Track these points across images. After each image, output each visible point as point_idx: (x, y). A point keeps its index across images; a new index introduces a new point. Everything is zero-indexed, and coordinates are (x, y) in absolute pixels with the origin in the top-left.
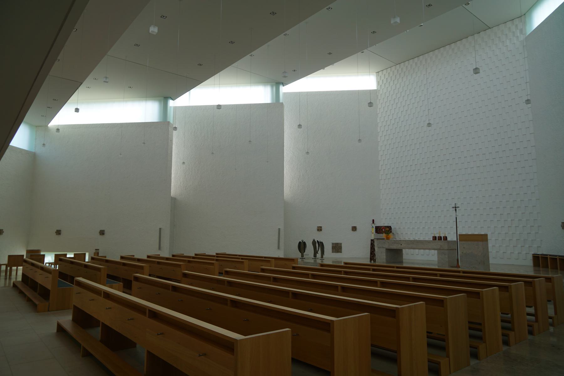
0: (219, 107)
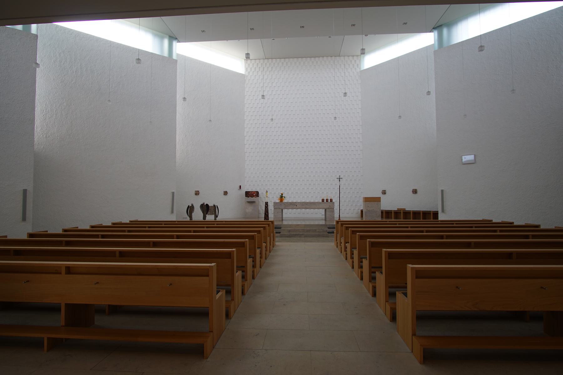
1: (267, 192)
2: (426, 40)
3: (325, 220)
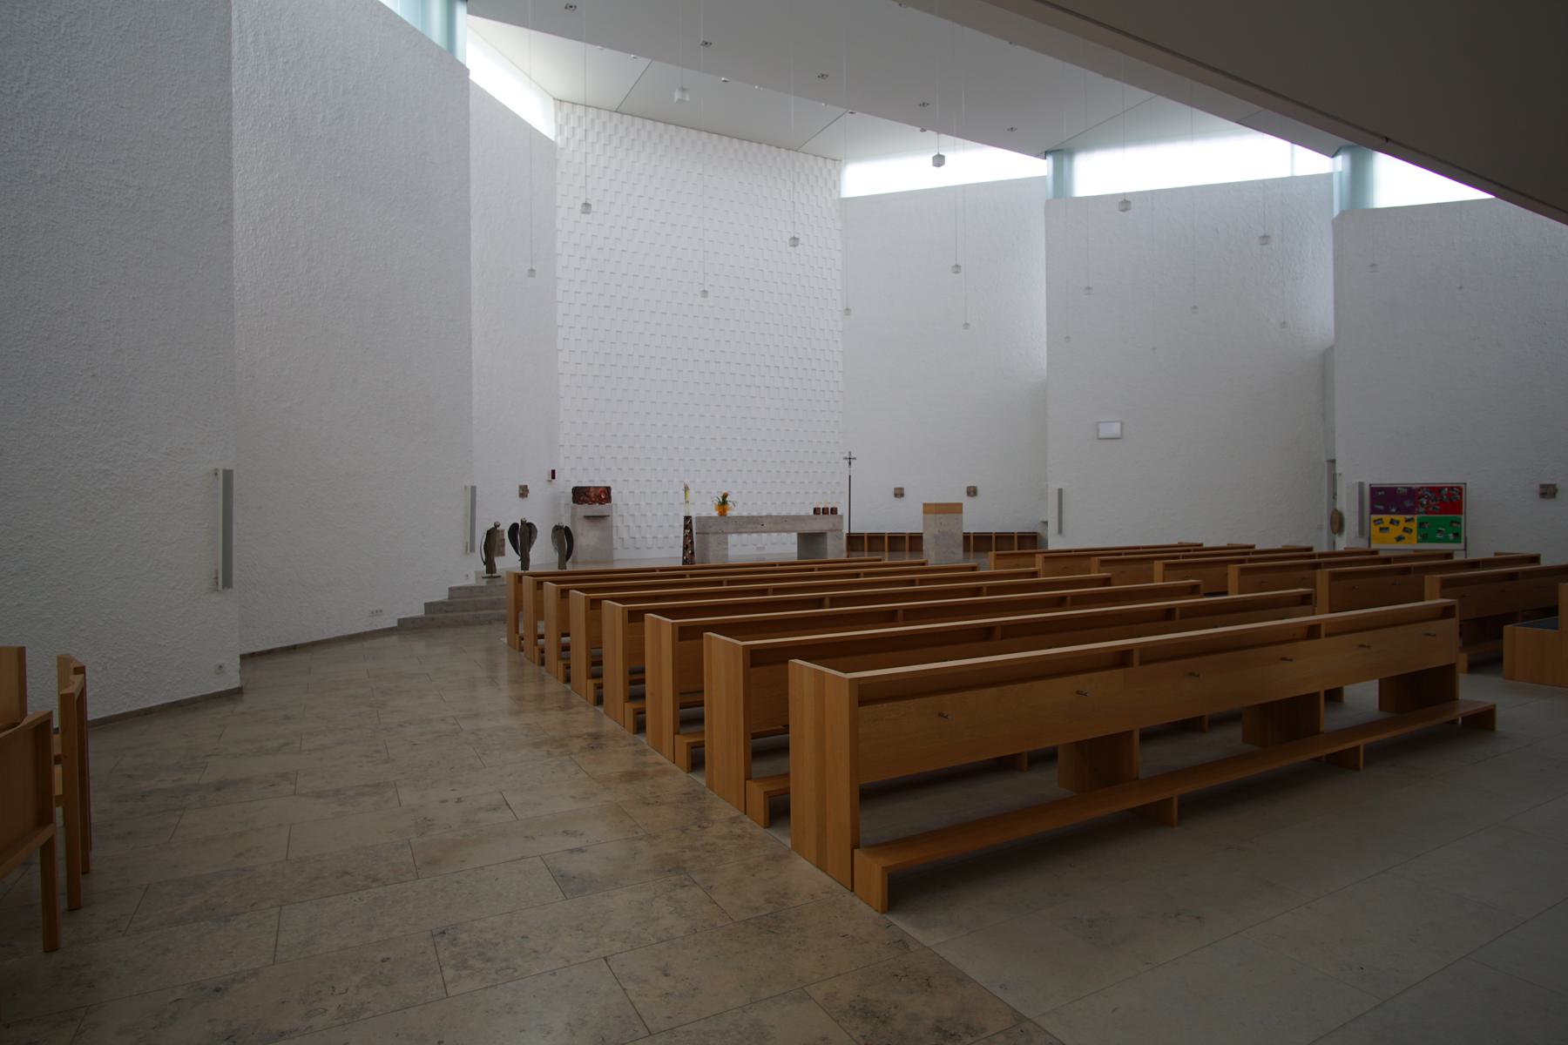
1: (686, 489)
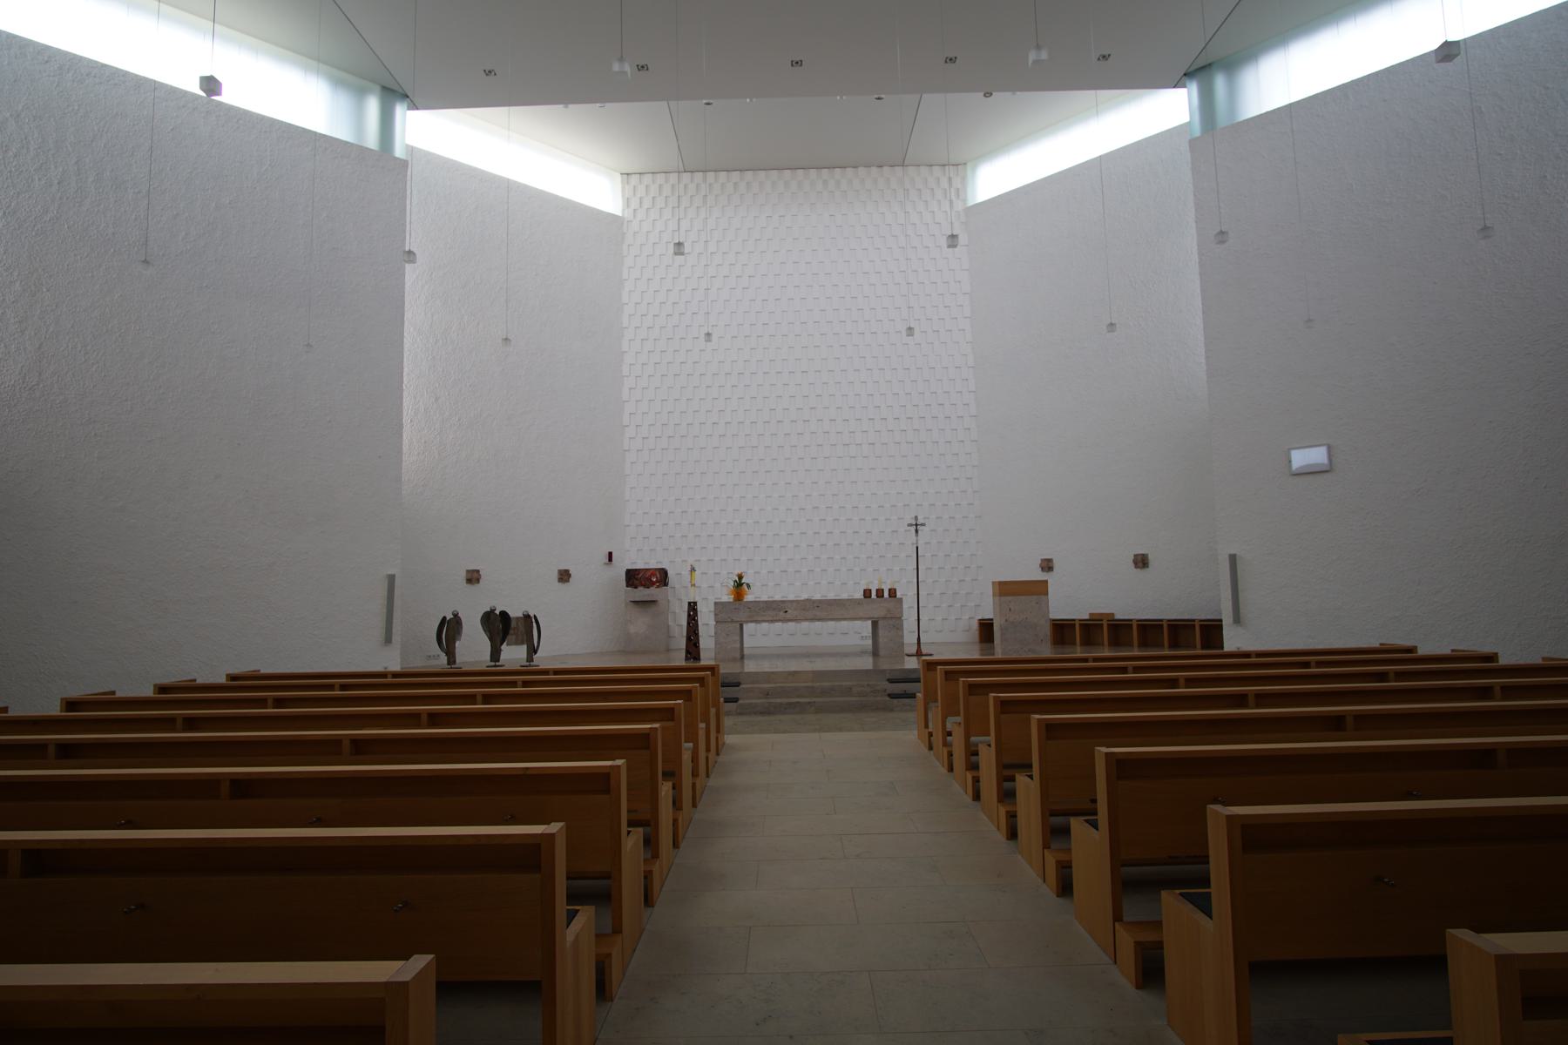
0: (1448, 51)
1: (693, 569)
2: (1167, 109)
3: (875, 653)
